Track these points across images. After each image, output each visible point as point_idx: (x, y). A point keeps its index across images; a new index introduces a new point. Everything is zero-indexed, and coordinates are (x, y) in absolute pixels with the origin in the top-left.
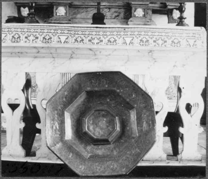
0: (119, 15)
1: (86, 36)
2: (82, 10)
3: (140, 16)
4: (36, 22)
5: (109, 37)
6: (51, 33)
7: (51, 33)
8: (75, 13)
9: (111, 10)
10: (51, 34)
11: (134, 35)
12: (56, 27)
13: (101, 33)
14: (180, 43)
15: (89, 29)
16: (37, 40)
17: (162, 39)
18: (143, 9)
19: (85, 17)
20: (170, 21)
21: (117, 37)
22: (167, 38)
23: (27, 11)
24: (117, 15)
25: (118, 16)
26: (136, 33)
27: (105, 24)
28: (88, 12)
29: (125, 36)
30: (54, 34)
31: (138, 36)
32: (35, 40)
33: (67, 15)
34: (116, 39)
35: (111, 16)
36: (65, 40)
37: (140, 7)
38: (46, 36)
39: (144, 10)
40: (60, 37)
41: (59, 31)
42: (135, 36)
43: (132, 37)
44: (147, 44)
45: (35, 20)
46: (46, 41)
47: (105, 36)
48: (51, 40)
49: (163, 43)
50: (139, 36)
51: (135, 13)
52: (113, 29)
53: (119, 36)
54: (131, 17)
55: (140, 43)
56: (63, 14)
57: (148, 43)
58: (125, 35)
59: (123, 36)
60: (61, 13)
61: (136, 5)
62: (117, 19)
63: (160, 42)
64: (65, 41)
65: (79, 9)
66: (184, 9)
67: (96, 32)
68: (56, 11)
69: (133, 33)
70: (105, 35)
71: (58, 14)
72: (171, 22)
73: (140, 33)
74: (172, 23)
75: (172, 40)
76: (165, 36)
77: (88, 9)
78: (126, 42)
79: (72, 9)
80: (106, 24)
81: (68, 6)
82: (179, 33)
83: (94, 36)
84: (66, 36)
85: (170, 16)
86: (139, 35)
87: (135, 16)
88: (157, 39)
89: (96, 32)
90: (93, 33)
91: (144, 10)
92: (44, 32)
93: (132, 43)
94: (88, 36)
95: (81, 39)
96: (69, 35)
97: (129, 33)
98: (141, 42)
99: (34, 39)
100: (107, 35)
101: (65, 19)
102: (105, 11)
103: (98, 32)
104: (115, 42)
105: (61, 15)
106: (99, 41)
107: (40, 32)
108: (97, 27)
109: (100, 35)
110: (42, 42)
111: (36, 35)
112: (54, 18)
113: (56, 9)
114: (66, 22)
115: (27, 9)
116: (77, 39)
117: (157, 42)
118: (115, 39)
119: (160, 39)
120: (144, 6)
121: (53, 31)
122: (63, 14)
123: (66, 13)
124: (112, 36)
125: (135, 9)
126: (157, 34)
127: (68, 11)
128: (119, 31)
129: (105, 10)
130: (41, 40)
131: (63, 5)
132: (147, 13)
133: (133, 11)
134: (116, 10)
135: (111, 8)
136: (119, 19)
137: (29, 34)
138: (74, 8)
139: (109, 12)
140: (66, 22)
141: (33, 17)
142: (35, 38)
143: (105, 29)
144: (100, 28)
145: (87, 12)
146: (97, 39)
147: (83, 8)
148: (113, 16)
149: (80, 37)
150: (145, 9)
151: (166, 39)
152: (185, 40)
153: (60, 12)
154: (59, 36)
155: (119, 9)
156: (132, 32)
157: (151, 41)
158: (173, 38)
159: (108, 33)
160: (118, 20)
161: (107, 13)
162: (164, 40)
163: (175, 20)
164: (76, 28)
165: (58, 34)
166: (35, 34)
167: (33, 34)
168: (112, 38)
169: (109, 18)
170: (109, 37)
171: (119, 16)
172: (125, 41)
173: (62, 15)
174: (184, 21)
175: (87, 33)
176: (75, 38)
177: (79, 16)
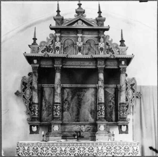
16: (48, 150)
17: (83, 147)
23: (35, 128)
25: (89, 130)
26: (67, 145)
29: (61, 146)
36: (27, 148)
38: (72, 148)
44: (128, 150)
51: (99, 128)
53: (21, 146)
56: (57, 130)
62: (89, 132)
63: (118, 148)
64: (101, 149)
71: (54, 130)
84: (64, 147)
92: (78, 146)
93: (28, 150)
106: (83, 149)
107: (130, 145)
111: (84, 147)
113: (53, 127)
115: (36, 127)
116: (53, 148)
119: (45, 147)
122: (57, 130)
127: (60, 128)
129: (83, 126)
130: (123, 149)
133: (98, 127)
135: (86, 125)
137: (116, 145)
140: (59, 135)
149: (110, 147)
152: (131, 147)
155: (90, 125)
166: (119, 145)
170: (71, 147)
173: (57, 131)
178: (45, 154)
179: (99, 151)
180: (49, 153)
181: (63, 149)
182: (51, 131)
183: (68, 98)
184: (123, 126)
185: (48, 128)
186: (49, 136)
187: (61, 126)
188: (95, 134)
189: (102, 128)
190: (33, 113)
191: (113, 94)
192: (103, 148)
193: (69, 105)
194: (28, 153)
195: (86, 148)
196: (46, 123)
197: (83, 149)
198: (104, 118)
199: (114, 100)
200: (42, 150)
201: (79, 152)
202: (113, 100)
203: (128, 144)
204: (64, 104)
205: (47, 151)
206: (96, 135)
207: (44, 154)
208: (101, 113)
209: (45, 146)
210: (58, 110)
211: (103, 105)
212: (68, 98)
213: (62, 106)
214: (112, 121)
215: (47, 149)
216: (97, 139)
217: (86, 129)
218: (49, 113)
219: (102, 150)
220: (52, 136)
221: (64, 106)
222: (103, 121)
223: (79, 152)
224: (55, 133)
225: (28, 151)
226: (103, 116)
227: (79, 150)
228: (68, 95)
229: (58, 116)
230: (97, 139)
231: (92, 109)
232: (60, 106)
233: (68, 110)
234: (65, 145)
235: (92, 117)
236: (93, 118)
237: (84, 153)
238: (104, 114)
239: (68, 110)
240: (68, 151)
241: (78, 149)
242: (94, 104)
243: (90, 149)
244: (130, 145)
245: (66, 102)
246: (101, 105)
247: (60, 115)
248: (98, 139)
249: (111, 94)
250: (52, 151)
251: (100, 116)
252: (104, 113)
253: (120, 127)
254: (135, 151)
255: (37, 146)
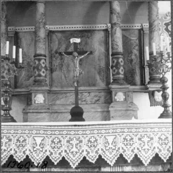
0: (99, 99)
1: (64, 136)
2: (61, 96)
3: (121, 100)
4: (10, 120)
5: (89, 136)
6: (25, 133)
7: (25, 133)
8: (53, 100)
9: (90, 94)
10: (25, 135)
11: (117, 133)
12: (31, 127)
13: (80, 132)
14: (168, 139)
15: (67, 127)
17: (148, 135)
18: (124, 92)
19: (65, 103)
20: (153, 104)
21: (98, 136)
22: (153, 134)
24: (97, 100)
25: (98, 100)
26: (119, 130)
27: (83, 120)
28: (67, 98)
30: (29, 135)
31: (121, 134)
32: (8, 143)
33: (46, 103)
34: (97, 139)
35: (91, 101)
37: (120, 91)
39: (124, 93)
40: (36, 138)
41: (34, 132)
42: (117, 134)
43: (115, 135)
45: (10, 118)
46: (19, 144)
47: (85, 136)
48: (25, 143)
49: (149, 141)
50: (122, 133)
51: (116, 98)
52: (93, 127)
53: (100, 135)
54: (112, 102)
55: (124, 142)
57: (132, 141)
58: (107, 133)
59: (104, 135)
60: (39, 101)
61: (116, 89)
62: (97, 103)
63: (146, 139)
65: (59, 94)
66: (167, 96)
67: (74, 131)
68: (35, 99)
69: (115, 131)
70: (85, 134)
71: (36, 102)
72: (154, 105)
73: (122, 130)
74: (154, 106)
75: (158, 136)
76: (150, 132)
77: (67, 94)
78: (108, 142)
79: (52, 95)
80: (85, 120)
81: (46, 93)
82: (166, 127)
83: (72, 136)
84: (42, 137)
85: (151, 98)
86: (122, 132)
87: (116, 101)
88: (143, 135)
89: (74, 131)
90: (71, 133)
91: (125, 94)
94: (66, 137)
95: (58, 140)
96: (45, 136)
97: (110, 131)
98: (124, 140)
99: (7, 142)
100: (86, 134)
101: (44, 108)
102: (85, 96)
103: (77, 131)
104: (95, 142)
105: (40, 102)
106: (149, 139)
107: (14, 133)
108: (75, 126)
109: (79, 134)
110: (16, 145)
112: (32, 107)
113: (35, 96)
114: (45, 111)
116: (54, 140)
117: (142, 139)
118: (96, 138)
120: (124, 89)
121: (27, 132)
122: (42, 102)
123: (45, 101)
124: (92, 135)
125: (115, 93)
126: (141, 130)
128: (99, 129)
129: (85, 94)
131: (41, 92)
132: (128, 96)
133: (113, 95)
134: (95, 94)
136: (99, 104)
138: (53, 93)
139: (88, 96)
140: (45, 111)
141: (8, 113)
142: (8, 141)
143: (84, 127)
144: (79, 126)
145: (66, 97)
146: (76, 139)
147: (63, 93)
148: (94, 101)
150: (125, 93)
151: (152, 136)
153: (39, 100)
154: (34, 138)
156: (114, 129)
157: (136, 139)
158: (160, 133)
159: (88, 132)
160: (98, 105)
161: (87, 98)
162: (150, 137)
163: (157, 102)
164: (53, 127)
165: (33, 135)
167: (6, 136)
168: (93, 138)
169: (90, 102)
170: (89, 136)
171: (100, 100)
172: (106, 141)
173: (41, 103)
174: (169, 109)
175: (65, 132)
176: (51, 139)
177: (58, 102)
178: (148, 150)
179: (109, 147)
180: (11, 147)
181: (110, 139)
182: (31, 104)
183: (59, 48)
184: (156, 93)
185: (27, 99)
186: (28, 113)
187: (48, 96)
188: (108, 108)
189: (120, 97)
190: (37, 73)
191: (136, 40)
192: (45, 140)
193: (62, 61)
194: (42, 151)
195: (83, 139)
196: (23, 90)
197: (78, 142)
198: (123, 80)
199: (137, 50)
200: (70, 145)
201: (142, 145)
202: (135, 49)
203: (131, 132)
204: (54, 59)
205: (79, 145)
206: (110, 109)
207: (146, 150)
208: (118, 70)
209: (163, 133)
210: (42, 66)
211: (120, 56)
212: (61, 48)
213: (51, 63)
214: (134, 84)
215: (78, 142)
216: (113, 117)
217: (92, 99)
218: (30, 75)
219: (43, 144)
220: (33, 112)
221: (54, 63)
222: (121, 84)
223: (142, 145)
224: (38, 107)
225: (42, 146)
226: (122, 76)
227: (140, 142)
228: (60, 43)
229: (42, 78)
230: (113, 117)
231: (100, 66)
232: (45, 60)
233: (61, 69)
234: (76, 132)
235: (100, 79)
236: (103, 82)
237: (79, 150)
238: (122, 73)
239: (62, 70)
240: (14, 143)
241: (140, 139)
242: (104, 57)
243: (54, 142)
244: (14, 133)
245: (56, 55)
246: (118, 56)
247: (46, 76)
248: (114, 117)
249: (133, 40)
250: (125, 142)
251: (116, 76)
252: (122, 70)
253: (152, 94)
254: (109, 145)
255: (60, 136)
